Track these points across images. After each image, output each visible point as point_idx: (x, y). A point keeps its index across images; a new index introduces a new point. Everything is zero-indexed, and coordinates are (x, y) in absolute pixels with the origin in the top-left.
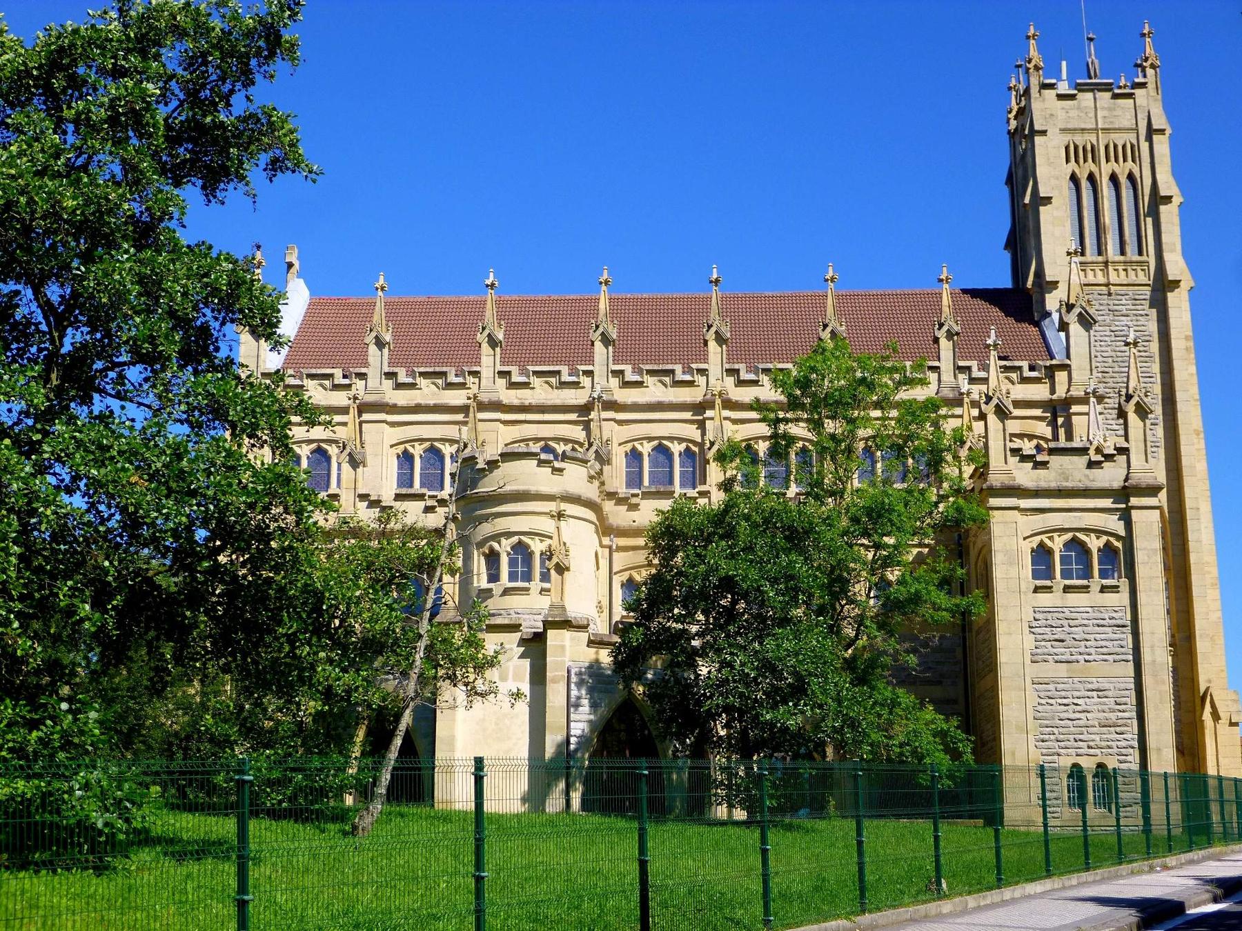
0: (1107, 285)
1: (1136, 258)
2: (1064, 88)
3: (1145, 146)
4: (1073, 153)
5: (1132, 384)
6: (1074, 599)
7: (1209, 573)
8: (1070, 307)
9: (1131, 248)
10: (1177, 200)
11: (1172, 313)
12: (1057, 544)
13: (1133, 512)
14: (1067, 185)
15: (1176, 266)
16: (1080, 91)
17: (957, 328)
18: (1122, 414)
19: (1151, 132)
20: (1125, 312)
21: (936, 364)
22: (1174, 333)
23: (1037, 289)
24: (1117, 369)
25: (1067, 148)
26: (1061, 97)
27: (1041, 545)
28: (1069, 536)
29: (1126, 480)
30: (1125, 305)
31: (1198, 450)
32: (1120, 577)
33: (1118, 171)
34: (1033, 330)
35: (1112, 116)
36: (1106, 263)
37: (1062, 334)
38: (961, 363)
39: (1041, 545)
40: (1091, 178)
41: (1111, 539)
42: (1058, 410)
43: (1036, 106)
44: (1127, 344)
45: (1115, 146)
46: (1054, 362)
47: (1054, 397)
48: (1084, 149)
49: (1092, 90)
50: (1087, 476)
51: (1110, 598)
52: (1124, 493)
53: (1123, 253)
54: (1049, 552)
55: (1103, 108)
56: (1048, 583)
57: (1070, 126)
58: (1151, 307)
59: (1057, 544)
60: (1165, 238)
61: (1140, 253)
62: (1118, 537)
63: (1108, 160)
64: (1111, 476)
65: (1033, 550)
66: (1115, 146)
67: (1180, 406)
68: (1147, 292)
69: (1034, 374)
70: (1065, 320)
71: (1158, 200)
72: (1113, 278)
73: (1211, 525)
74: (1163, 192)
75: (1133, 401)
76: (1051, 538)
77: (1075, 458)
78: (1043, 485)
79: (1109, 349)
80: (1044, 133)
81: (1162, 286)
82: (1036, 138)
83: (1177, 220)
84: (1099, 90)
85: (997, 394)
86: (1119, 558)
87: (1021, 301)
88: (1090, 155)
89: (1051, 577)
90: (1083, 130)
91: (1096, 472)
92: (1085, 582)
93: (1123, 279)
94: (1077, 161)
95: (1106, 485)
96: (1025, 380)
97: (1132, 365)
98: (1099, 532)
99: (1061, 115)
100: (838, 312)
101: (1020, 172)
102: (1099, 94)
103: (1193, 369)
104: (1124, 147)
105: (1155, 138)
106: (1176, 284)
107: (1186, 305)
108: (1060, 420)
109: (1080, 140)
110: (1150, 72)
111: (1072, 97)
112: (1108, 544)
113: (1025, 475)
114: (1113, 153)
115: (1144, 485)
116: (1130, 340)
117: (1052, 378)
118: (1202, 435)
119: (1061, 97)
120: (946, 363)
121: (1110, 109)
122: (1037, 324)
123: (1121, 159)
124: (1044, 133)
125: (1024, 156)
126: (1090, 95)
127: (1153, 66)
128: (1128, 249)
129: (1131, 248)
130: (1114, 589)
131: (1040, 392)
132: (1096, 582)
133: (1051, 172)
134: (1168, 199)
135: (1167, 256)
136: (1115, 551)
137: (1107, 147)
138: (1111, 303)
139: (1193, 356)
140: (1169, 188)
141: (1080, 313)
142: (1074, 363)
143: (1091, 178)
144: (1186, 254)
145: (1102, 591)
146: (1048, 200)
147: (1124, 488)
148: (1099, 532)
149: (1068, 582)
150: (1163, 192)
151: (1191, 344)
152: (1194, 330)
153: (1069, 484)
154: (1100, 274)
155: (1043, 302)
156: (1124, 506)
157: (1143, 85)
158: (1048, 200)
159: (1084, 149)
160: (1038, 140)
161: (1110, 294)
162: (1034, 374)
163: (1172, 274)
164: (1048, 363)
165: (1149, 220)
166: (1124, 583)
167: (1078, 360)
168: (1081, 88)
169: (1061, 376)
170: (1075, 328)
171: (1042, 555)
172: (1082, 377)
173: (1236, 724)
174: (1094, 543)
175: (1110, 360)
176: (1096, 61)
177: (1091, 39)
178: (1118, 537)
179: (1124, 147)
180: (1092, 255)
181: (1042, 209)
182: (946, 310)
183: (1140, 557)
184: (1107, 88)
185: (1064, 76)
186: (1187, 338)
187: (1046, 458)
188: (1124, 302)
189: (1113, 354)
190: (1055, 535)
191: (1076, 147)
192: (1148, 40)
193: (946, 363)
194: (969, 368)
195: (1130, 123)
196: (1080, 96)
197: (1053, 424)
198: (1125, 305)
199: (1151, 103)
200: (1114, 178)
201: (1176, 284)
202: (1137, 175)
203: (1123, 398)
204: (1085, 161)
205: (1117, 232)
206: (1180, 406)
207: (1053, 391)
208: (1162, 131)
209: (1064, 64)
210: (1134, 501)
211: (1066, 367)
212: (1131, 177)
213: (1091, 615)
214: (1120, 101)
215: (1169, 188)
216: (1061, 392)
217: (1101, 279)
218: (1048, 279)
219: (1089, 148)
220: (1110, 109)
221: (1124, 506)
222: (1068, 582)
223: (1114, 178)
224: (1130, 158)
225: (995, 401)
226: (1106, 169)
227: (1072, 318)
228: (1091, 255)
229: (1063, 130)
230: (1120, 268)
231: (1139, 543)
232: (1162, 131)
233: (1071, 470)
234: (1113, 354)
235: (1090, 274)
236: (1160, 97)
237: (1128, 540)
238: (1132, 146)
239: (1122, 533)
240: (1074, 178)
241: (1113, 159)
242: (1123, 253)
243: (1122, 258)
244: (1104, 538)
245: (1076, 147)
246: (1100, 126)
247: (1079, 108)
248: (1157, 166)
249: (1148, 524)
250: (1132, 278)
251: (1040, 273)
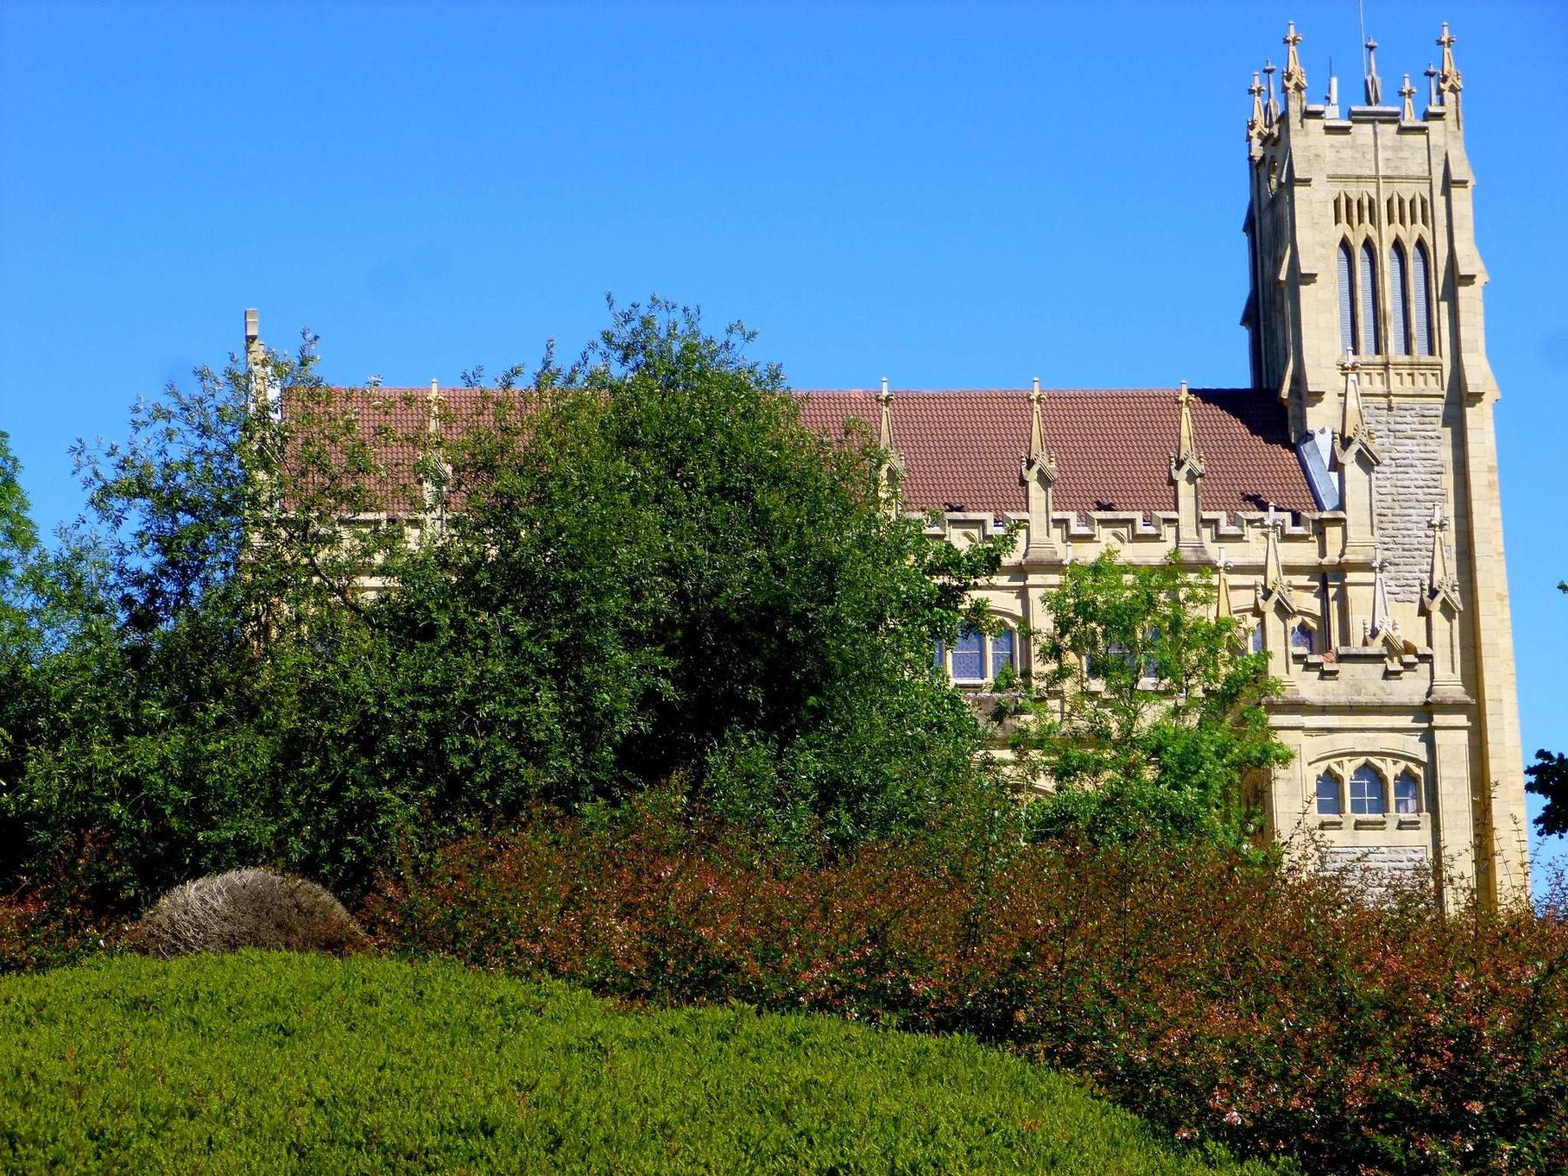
0: (1387, 396)
1: (1430, 359)
2: (1333, 115)
3: (1440, 201)
4: (1345, 210)
5: (1438, 576)
6: (1369, 838)
7: (1513, 783)
8: (1346, 442)
9: (1419, 344)
10: (1480, 280)
11: (1471, 436)
12: (1347, 771)
13: (1349, 589)
14: (1335, 253)
15: (1478, 374)
16: (1355, 121)
17: (1200, 468)
18: (1424, 611)
19: (1448, 183)
20: (1409, 433)
21: (1173, 515)
22: (1473, 464)
23: (1296, 401)
24: (1397, 511)
25: (1337, 202)
26: (1329, 130)
27: (1329, 771)
28: (1362, 760)
29: (1429, 694)
30: (1410, 423)
31: (1502, 620)
32: (1419, 811)
33: (1403, 237)
34: (1289, 455)
35: (1395, 159)
36: (1386, 365)
37: (1334, 476)
38: (1206, 515)
39: (1329, 771)
40: (1368, 245)
41: (1411, 765)
42: (1328, 577)
43: (1297, 142)
44: (1431, 526)
45: (1401, 202)
46: (1325, 515)
47: (1325, 561)
48: (1360, 203)
49: (1372, 122)
50: (1383, 688)
51: (1410, 836)
52: (1426, 711)
53: (1408, 351)
54: (1338, 780)
55: (1385, 147)
56: (1335, 818)
57: (1341, 172)
58: (1445, 424)
59: (1347, 771)
60: (1464, 333)
61: (1431, 352)
62: (1418, 763)
63: (1390, 221)
64: (1411, 688)
65: (1319, 778)
66: (1401, 202)
67: (1480, 563)
68: (1439, 406)
69: (1299, 530)
70: (1340, 459)
71: (1455, 279)
72: (1395, 386)
73: (1516, 721)
74: (1463, 271)
75: (1439, 598)
76: (1340, 764)
77: (1369, 666)
78: (1332, 699)
79: (1387, 483)
80: (1306, 182)
81: (1459, 399)
82: (1297, 189)
83: (1480, 307)
84: (1382, 122)
85: (1278, 588)
86: (1421, 785)
87: (1267, 407)
88: (1366, 214)
89: (1340, 810)
90: (1358, 177)
91: (1393, 684)
92: (1379, 817)
93: (1408, 387)
94: (1349, 222)
95: (1405, 700)
96: (1287, 538)
97: (1438, 552)
98: (1396, 757)
99: (1329, 155)
100: (1049, 443)
101: (1268, 227)
102: (1381, 127)
103: (1497, 512)
104: (1412, 202)
105: (1455, 191)
106: (1478, 397)
107: (1489, 426)
108: (1332, 592)
109: (1354, 190)
110: (1449, 97)
111: (1345, 130)
112: (1407, 771)
113: (1308, 687)
114: (1399, 211)
115: (1450, 701)
116: (1436, 521)
117: (1321, 535)
118: (1507, 602)
119: (1329, 130)
120: (1186, 512)
121: (1396, 149)
122: (1294, 448)
123: (1408, 220)
124: (1306, 182)
125: (1274, 202)
126: (1369, 127)
127: (1453, 89)
128: (1415, 346)
129: (1419, 344)
130: (1414, 825)
131: (1306, 553)
132: (1393, 816)
133: (1315, 236)
134: (1469, 279)
135: (1466, 358)
136: (1415, 779)
137: (1390, 202)
138: (1391, 420)
139: (1497, 493)
140: (1471, 263)
141: (1360, 451)
142: (1350, 515)
143: (1368, 245)
144: (1492, 355)
145: (1399, 828)
146: (1311, 278)
147: (1427, 704)
148: (1396, 757)
149: (1360, 817)
150: (1463, 271)
151: (1495, 477)
152: (1500, 460)
153: (1362, 699)
154: (1377, 379)
155: (1302, 418)
156: (1426, 725)
157: (1439, 116)
158: (1311, 278)
159: (1360, 203)
160: (1299, 191)
161: (1390, 408)
162: (1299, 530)
163: (1473, 383)
164: (1317, 515)
165: (1444, 305)
166: (1425, 817)
167: (1356, 512)
168: (1356, 117)
169: (1333, 533)
170: (1353, 470)
171: (1330, 782)
172: (1358, 536)
173: (753, 335)
174: (1391, 770)
175: (1389, 498)
176: (1378, 80)
177: (1371, 48)
178: (1418, 763)
179: (1412, 202)
180: (1367, 353)
181: (1303, 288)
182: (1185, 441)
183: (1444, 787)
184: (1392, 118)
185: (1334, 99)
186: (1490, 470)
187: (1334, 667)
188: (1409, 419)
189: (1394, 490)
190: (1345, 759)
191: (1348, 201)
192: (1447, 50)
193: (1186, 512)
194: (1216, 522)
195: (1419, 169)
196: (1356, 128)
197: (1322, 594)
198: (1410, 423)
199: (1450, 141)
200: (1398, 246)
201: (1478, 397)
202: (1429, 242)
203: (1426, 593)
204: (1361, 221)
205: (1401, 324)
206: (1479, 563)
207: (1323, 554)
208: (1463, 183)
209: (1334, 81)
210: (1438, 719)
211: (1340, 522)
212: (1420, 244)
213: (1387, 856)
214: (1408, 138)
215: (1471, 263)
216: (1333, 556)
217: (1378, 387)
218: (1311, 389)
219: (1366, 203)
220: (1396, 149)
221: (1426, 725)
222: (1360, 817)
223: (1398, 246)
224: (1419, 220)
225: (1275, 597)
226: (1388, 233)
227: (1348, 458)
228: (1366, 354)
229: (1333, 177)
230: (1405, 372)
231: (1443, 771)
232: (1463, 183)
233: (1364, 681)
234: (1394, 490)
235: (1365, 379)
236: (1461, 133)
237: (1431, 767)
238: (1423, 202)
239: (1424, 758)
240: (1345, 245)
241: (1397, 218)
242: (1408, 351)
243: (1407, 359)
244: (1403, 764)
245: (1348, 201)
246: (1381, 173)
247: (1353, 147)
248: (1455, 232)
249: (1453, 744)
250: (1420, 386)
251: (1299, 379)
